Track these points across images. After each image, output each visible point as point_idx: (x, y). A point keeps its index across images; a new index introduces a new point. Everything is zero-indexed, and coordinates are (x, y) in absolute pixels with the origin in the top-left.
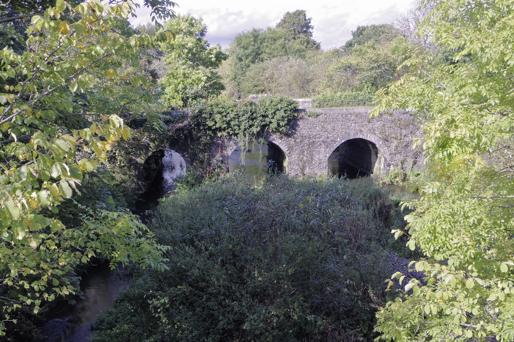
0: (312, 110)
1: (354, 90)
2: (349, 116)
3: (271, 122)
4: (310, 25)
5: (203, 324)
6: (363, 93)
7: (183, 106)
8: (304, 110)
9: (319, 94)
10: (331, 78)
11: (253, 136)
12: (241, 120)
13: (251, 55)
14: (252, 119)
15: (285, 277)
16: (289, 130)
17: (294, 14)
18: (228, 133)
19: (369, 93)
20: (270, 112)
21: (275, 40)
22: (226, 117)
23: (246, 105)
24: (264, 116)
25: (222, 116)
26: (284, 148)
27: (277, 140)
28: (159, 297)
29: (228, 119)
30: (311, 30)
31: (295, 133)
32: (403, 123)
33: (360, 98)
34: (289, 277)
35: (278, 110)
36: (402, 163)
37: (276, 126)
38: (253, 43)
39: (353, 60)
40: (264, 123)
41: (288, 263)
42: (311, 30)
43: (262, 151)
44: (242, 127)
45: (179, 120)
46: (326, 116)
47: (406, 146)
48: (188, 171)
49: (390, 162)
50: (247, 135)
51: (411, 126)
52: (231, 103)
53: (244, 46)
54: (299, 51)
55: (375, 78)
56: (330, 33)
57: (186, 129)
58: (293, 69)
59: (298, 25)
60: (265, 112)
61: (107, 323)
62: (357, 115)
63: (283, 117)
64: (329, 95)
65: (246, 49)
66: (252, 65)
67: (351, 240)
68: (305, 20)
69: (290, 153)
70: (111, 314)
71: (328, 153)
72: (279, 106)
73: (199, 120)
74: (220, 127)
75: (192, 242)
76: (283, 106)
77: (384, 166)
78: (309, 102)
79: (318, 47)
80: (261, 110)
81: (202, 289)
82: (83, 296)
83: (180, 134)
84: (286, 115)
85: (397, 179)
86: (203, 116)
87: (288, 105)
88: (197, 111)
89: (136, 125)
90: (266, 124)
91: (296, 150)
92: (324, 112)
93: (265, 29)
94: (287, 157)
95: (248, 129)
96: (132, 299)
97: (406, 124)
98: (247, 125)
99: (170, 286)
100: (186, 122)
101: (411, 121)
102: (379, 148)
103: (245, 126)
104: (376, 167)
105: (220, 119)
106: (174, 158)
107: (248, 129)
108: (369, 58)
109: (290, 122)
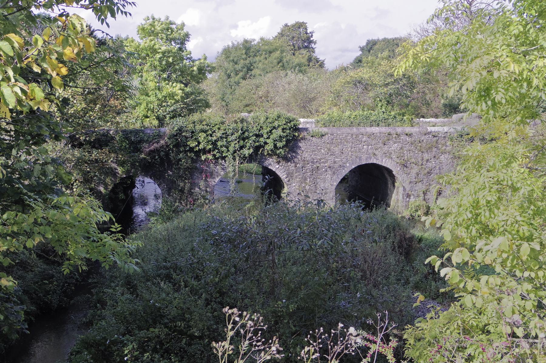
0: (316, 130)
1: (366, 109)
2: (360, 136)
3: (266, 143)
4: (312, 39)
6: (376, 112)
7: (159, 127)
8: (306, 129)
9: (323, 114)
10: (338, 95)
11: (244, 160)
12: (229, 140)
13: (242, 71)
14: (244, 139)
15: (285, 314)
16: (288, 153)
17: (293, 26)
19: (384, 112)
20: (264, 132)
21: (270, 52)
22: (211, 136)
23: (236, 122)
24: (257, 136)
25: (207, 135)
26: (282, 175)
27: (273, 165)
29: (214, 138)
30: (313, 45)
32: (424, 145)
33: (372, 119)
34: (291, 315)
35: (274, 128)
36: (425, 193)
37: (272, 147)
38: (244, 56)
39: (364, 73)
40: (257, 144)
41: (288, 299)
42: (313, 45)
43: (256, 182)
44: (231, 149)
47: (428, 173)
48: (165, 202)
49: (410, 193)
50: (237, 158)
51: (434, 149)
52: (218, 119)
53: (233, 60)
54: (300, 65)
55: (391, 95)
56: (335, 47)
57: (162, 151)
58: (293, 86)
59: (299, 39)
60: (259, 131)
62: (370, 135)
63: (280, 137)
65: (236, 63)
66: (243, 82)
67: (365, 272)
68: (307, 33)
71: (336, 180)
72: (276, 124)
73: (179, 140)
74: (204, 149)
75: (168, 278)
76: (280, 124)
77: (403, 198)
78: (311, 122)
79: (322, 65)
80: (255, 128)
82: (26, 329)
84: (285, 134)
85: (419, 213)
86: (184, 134)
87: (287, 122)
88: (176, 128)
90: (260, 145)
91: (296, 177)
92: (330, 132)
95: (239, 151)
96: (92, 346)
98: (237, 146)
99: (140, 329)
100: (162, 142)
102: (396, 175)
103: (235, 147)
104: (393, 198)
105: (205, 138)
106: (147, 187)
107: (239, 151)
108: (383, 71)
109: (290, 143)
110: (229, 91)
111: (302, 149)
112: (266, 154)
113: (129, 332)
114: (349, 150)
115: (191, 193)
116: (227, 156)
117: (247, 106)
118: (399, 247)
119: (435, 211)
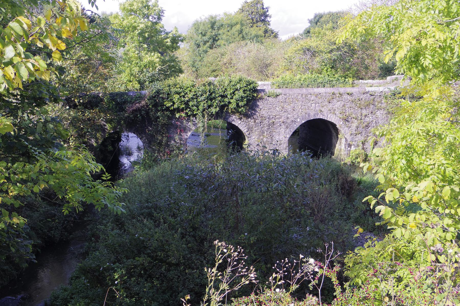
2: (309, 96)
3: (230, 103)
4: (267, 13)
5: (162, 296)
7: (140, 89)
8: (263, 91)
9: (278, 77)
11: (212, 117)
12: (199, 100)
13: (208, 42)
14: (211, 100)
18: (187, 113)
20: (229, 92)
22: (184, 97)
23: (204, 85)
24: (223, 96)
25: (181, 97)
28: (115, 269)
29: (187, 99)
30: (268, 19)
31: (255, 114)
33: (319, 81)
35: (237, 90)
36: (363, 144)
37: (235, 106)
39: (312, 42)
40: (223, 103)
41: (249, 232)
44: (201, 108)
45: (135, 100)
46: (285, 97)
49: (351, 143)
51: (371, 106)
53: (202, 33)
54: (257, 36)
55: (335, 60)
58: (252, 53)
60: (224, 92)
61: (61, 299)
63: (242, 97)
64: (288, 77)
68: (263, 9)
69: (249, 134)
70: (65, 290)
72: (238, 86)
73: (157, 100)
74: (178, 108)
75: (150, 215)
76: (242, 86)
77: (345, 148)
80: (220, 90)
81: (161, 261)
83: (137, 115)
84: (245, 95)
87: (247, 85)
89: (91, 106)
90: (225, 104)
92: (283, 93)
93: (222, 16)
94: (246, 138)
95: (207, 109)
96: (88, 272)
97: (366, 104)
98: (206, 105)
99: (128, 258)
100: (143, 103)
101: (372, 101)
102: (339, 129)
103: (204, 106)
104: (336, 148)
105: (178, 99)
106: (132, 141)
110: (198, 59)
111: (260, 107)
112: (230, 112)
113: (118, 261)
114: (300, 107)
115: (167, 145)
116: (197, 114)
117: (214, 71)
118: (342, 189)
119: (372, 158)
